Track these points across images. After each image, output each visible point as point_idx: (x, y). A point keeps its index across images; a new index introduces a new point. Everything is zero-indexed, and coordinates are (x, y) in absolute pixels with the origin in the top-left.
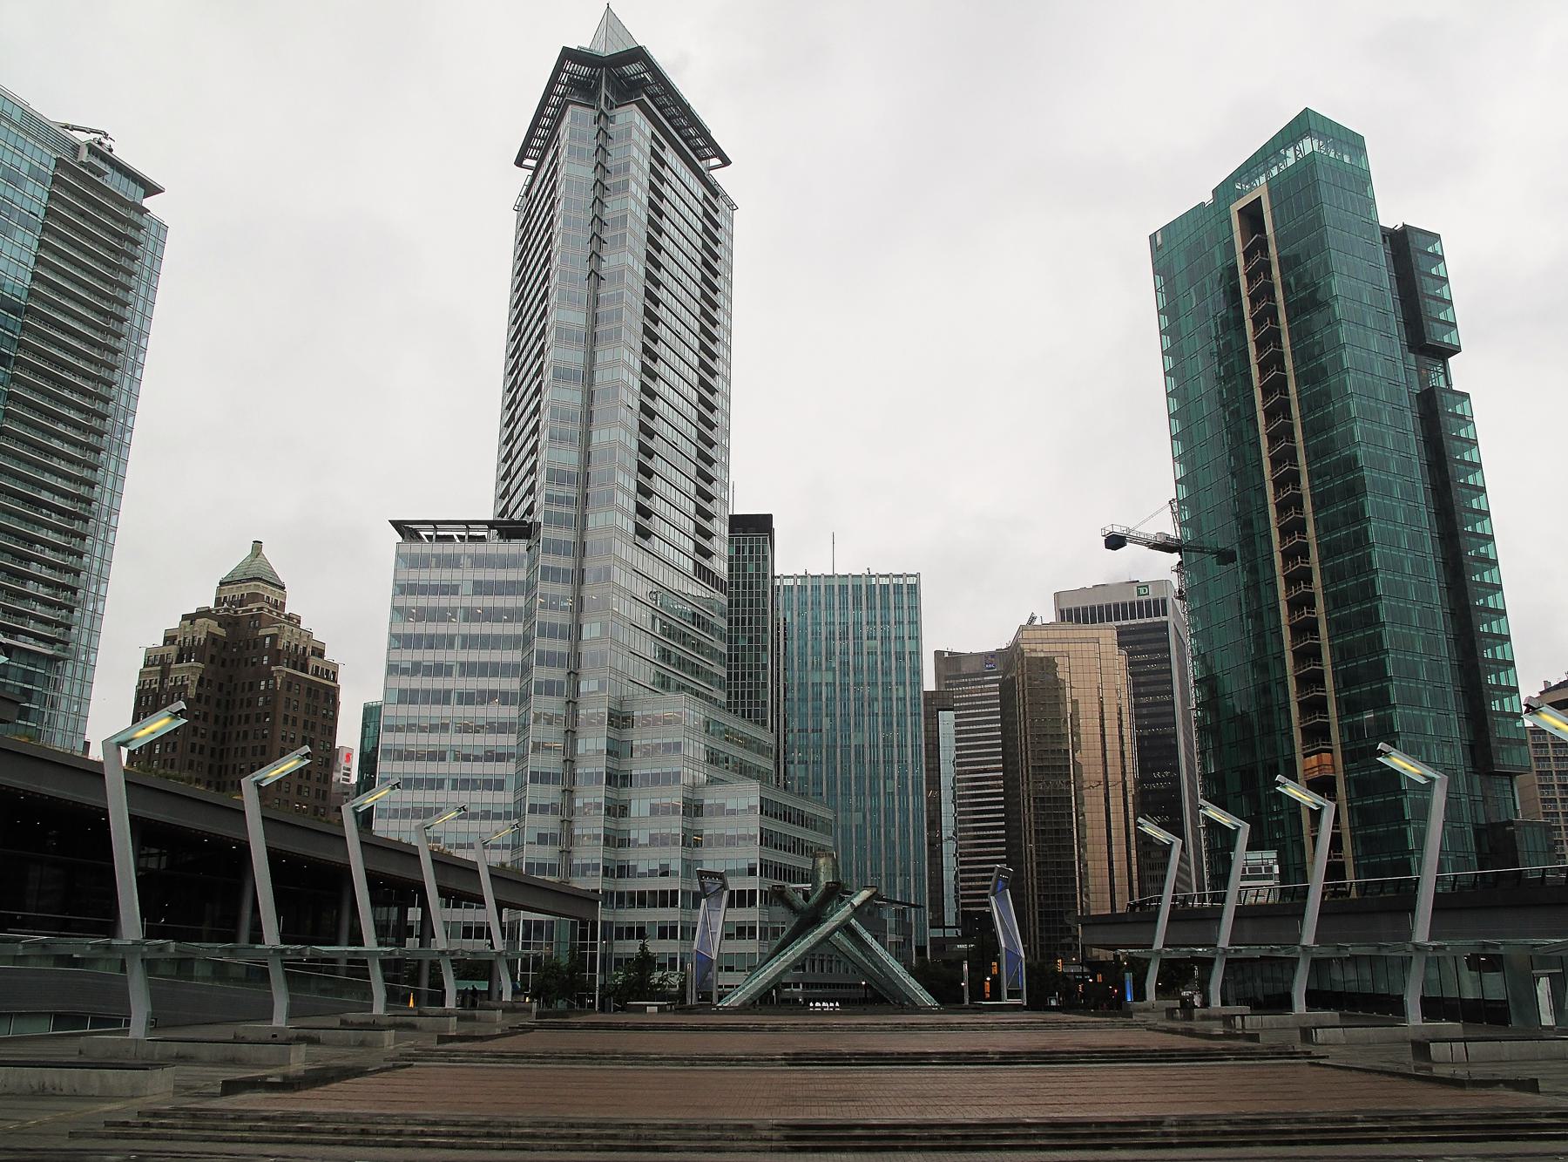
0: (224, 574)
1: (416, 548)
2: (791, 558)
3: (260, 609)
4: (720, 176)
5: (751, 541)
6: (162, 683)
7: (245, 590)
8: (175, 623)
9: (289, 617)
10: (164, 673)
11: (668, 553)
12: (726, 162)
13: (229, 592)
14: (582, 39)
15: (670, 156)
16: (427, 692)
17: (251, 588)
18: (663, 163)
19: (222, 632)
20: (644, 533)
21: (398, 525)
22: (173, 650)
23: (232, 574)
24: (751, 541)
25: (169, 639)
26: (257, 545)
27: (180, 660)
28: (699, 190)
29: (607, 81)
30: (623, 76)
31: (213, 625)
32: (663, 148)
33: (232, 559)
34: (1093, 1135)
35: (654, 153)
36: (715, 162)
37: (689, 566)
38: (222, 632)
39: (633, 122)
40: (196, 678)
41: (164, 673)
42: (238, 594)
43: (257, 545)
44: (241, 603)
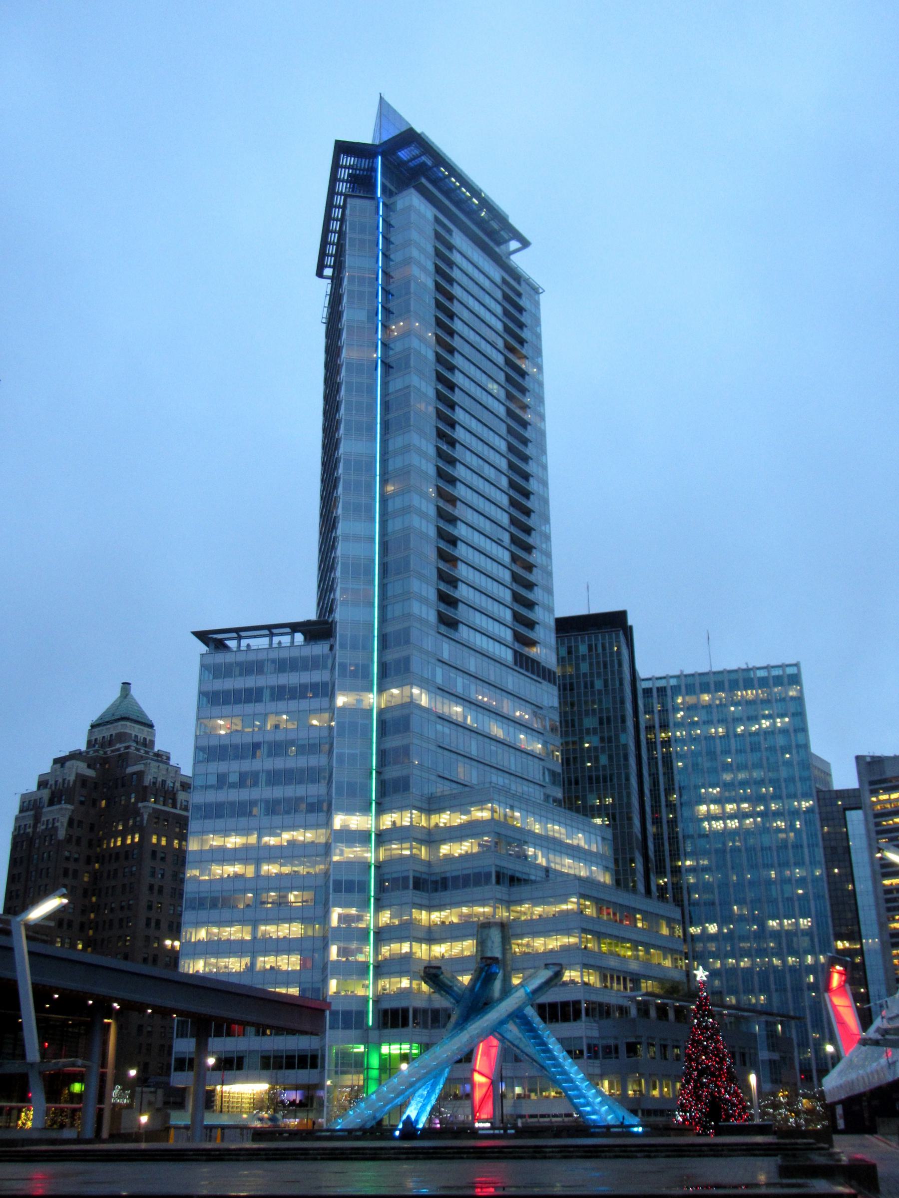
0: (94, 717)
1: (221, 658)
2: (656, 656)
3: (128, 747)
4: (521, 261)
5: (603, 639)
6: (35, 826)
7: (113, 730)
8: (46, 767)
9: (158, 755)
10: (37, 819)
11: (480, 642)
12: (525, 244)
13: (100, 734)
14: (364, 133)
15: (458, 239)
16: (232, 804)
17: (120, 727)
18: (451, 247)
19: (91, 773)
20: (448, 623)
21: (202, 636)
22: (46, 794)
23: (101, 718)
24: (603, 639)
25: (42, 783)
26: (126, 685)
27: (51, 803)
28: (496, 274)
29: (390, 172)
30: (402, 163)
31: (81, 767)
32: (449, 231)
33: (103, 701)
34: (510, 1153)
35: (438, 236)
36: (514, 245)
37: (508, 656)
38: (91, 773)
39: (415, 205)
40: (65, 820)
41: (37, 819)
42: (107, 734)
43: (126, 685)
44: (111, 743)
